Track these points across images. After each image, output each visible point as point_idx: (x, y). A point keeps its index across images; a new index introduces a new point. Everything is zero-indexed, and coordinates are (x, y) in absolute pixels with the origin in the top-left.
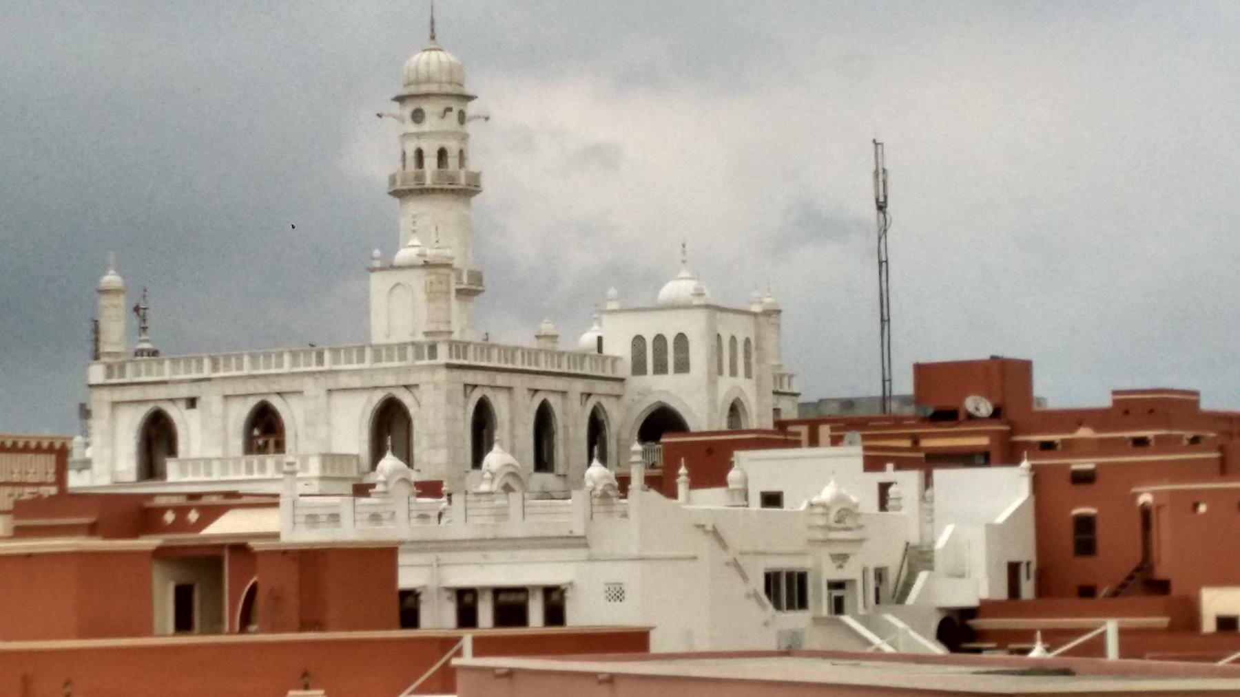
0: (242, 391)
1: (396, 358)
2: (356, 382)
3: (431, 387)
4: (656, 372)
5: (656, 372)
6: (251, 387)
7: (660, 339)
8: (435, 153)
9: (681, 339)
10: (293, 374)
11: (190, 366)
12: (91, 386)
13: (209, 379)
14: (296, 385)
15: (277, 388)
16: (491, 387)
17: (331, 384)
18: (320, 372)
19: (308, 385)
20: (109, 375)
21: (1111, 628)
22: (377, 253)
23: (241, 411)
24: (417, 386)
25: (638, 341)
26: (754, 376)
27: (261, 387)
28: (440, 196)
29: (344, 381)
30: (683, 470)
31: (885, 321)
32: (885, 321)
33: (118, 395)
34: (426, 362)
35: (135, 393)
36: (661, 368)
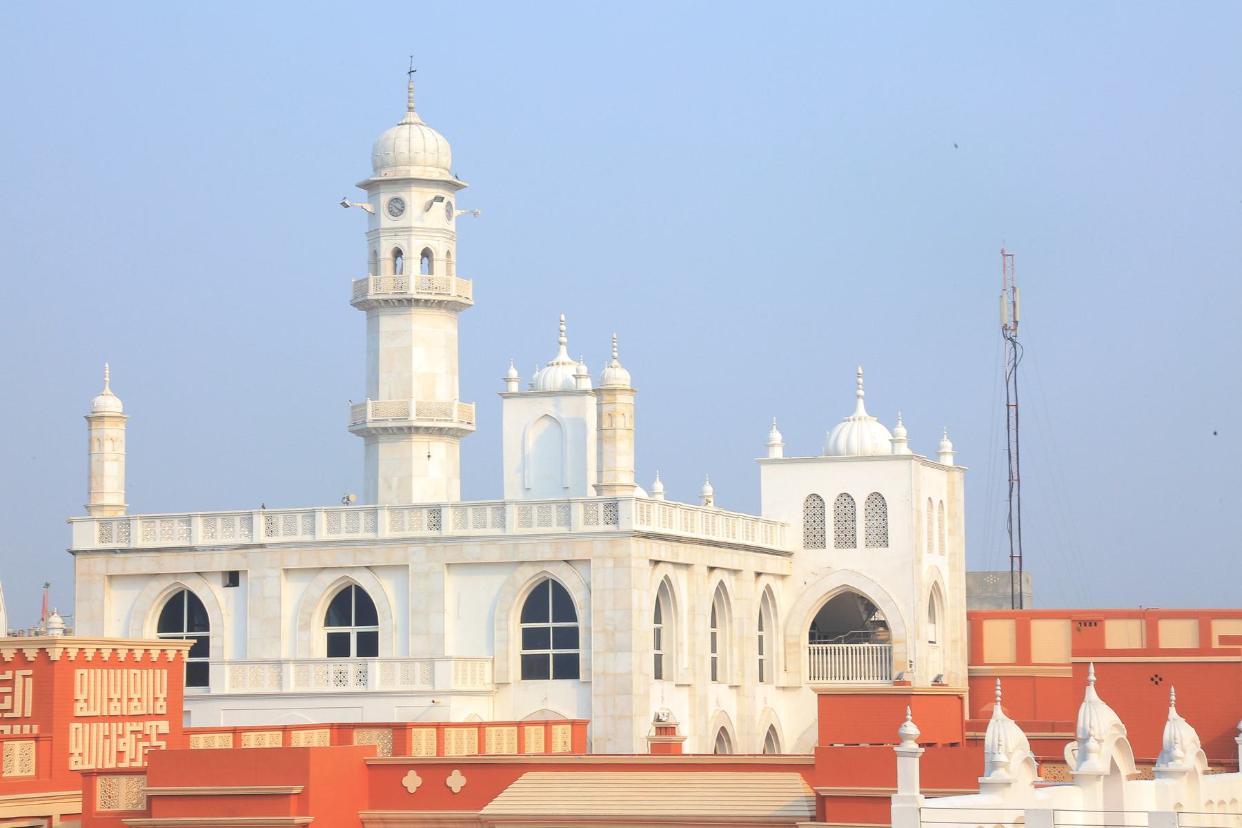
0: (167, 558)
1: (601, 520)
2: (493, 554)
3: (610, 563)
4: (839, 544)
5: (839, 544)
6: (327, 558)
7: (846, 500)
8: (417, 254)
9: (877, 501)
10: (395, 540)
11: (215, 526)
12: (74, 553)
13: (262, 546)
14: (397, 557)
15: (367, 561)
16: (676, 565)
17: (452, 555)
18: (435, 539)
19: (417, 557)
20: (104, 537)
21: (380, 756)
22: (513, 373)
23: (323, 592)
24: (587, 561)
25: (815, 501)
26: (947, 551)
27: (343, 558)
28: (435, 312)
29: (472, 552)
30: (1173, 690)
31: (1014, 479)
32: (1014, 479)
33: (117, 565)
34: (602, 527)
35: (146, 564)
36: (846, 539)
